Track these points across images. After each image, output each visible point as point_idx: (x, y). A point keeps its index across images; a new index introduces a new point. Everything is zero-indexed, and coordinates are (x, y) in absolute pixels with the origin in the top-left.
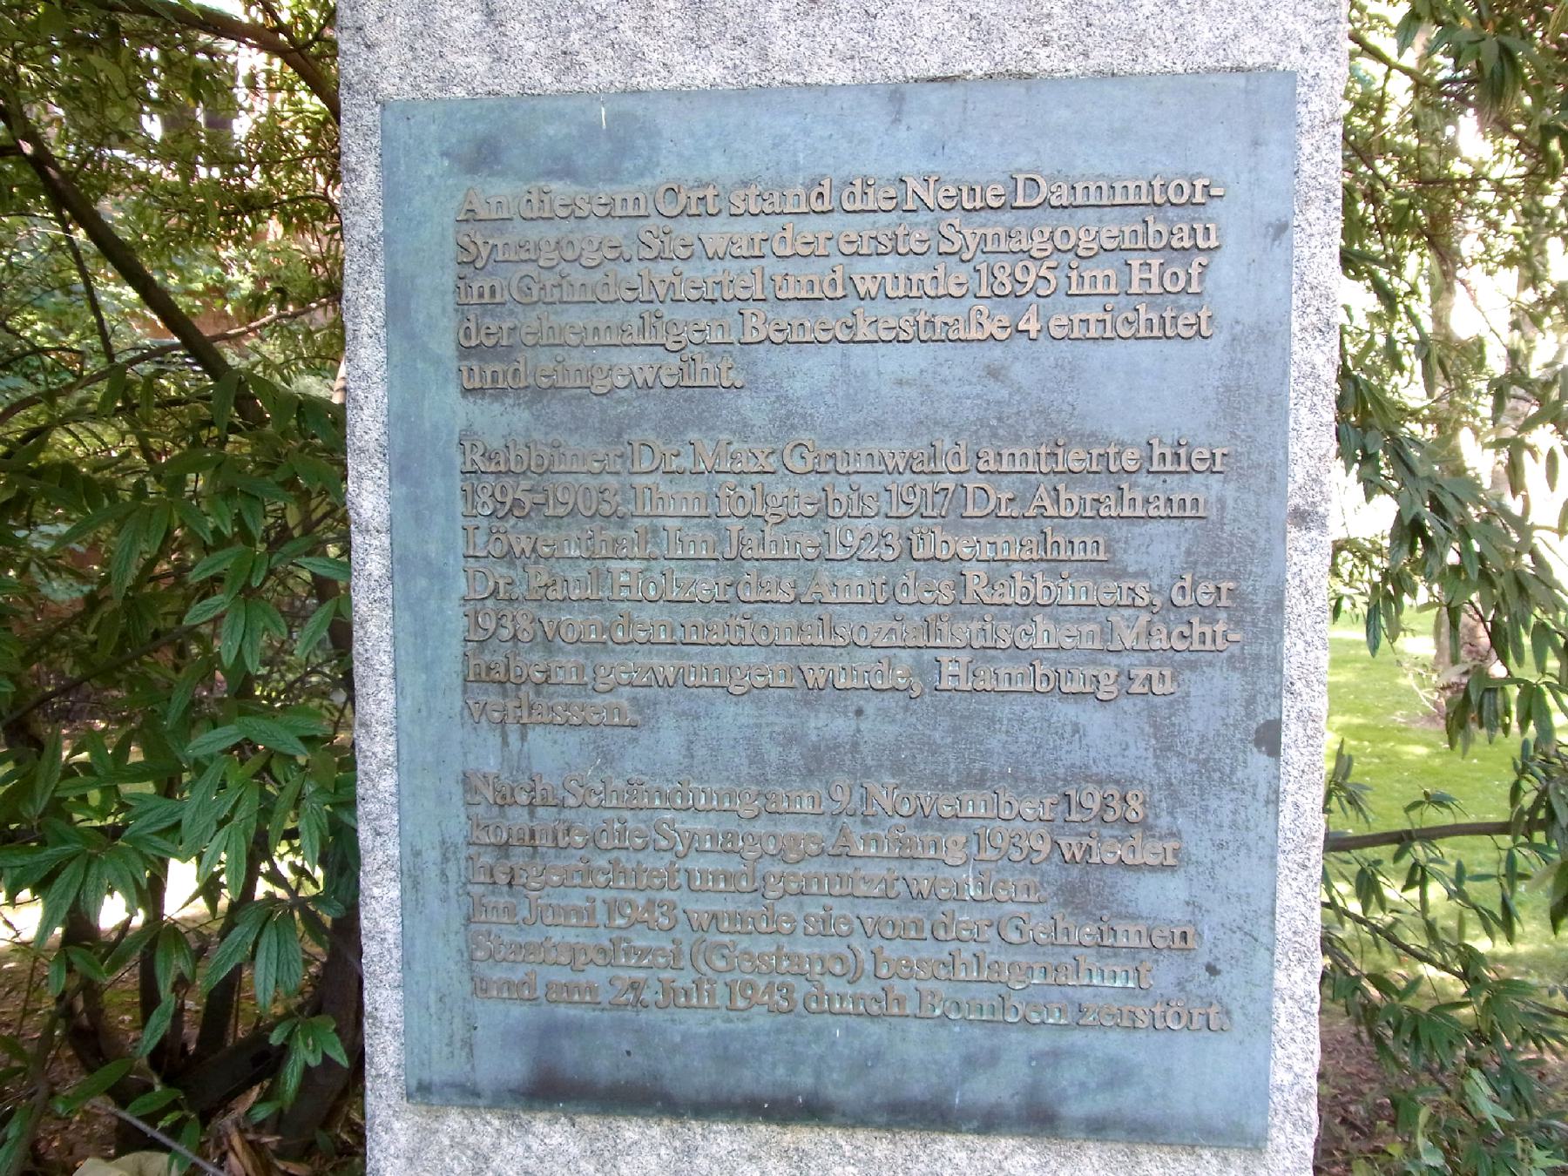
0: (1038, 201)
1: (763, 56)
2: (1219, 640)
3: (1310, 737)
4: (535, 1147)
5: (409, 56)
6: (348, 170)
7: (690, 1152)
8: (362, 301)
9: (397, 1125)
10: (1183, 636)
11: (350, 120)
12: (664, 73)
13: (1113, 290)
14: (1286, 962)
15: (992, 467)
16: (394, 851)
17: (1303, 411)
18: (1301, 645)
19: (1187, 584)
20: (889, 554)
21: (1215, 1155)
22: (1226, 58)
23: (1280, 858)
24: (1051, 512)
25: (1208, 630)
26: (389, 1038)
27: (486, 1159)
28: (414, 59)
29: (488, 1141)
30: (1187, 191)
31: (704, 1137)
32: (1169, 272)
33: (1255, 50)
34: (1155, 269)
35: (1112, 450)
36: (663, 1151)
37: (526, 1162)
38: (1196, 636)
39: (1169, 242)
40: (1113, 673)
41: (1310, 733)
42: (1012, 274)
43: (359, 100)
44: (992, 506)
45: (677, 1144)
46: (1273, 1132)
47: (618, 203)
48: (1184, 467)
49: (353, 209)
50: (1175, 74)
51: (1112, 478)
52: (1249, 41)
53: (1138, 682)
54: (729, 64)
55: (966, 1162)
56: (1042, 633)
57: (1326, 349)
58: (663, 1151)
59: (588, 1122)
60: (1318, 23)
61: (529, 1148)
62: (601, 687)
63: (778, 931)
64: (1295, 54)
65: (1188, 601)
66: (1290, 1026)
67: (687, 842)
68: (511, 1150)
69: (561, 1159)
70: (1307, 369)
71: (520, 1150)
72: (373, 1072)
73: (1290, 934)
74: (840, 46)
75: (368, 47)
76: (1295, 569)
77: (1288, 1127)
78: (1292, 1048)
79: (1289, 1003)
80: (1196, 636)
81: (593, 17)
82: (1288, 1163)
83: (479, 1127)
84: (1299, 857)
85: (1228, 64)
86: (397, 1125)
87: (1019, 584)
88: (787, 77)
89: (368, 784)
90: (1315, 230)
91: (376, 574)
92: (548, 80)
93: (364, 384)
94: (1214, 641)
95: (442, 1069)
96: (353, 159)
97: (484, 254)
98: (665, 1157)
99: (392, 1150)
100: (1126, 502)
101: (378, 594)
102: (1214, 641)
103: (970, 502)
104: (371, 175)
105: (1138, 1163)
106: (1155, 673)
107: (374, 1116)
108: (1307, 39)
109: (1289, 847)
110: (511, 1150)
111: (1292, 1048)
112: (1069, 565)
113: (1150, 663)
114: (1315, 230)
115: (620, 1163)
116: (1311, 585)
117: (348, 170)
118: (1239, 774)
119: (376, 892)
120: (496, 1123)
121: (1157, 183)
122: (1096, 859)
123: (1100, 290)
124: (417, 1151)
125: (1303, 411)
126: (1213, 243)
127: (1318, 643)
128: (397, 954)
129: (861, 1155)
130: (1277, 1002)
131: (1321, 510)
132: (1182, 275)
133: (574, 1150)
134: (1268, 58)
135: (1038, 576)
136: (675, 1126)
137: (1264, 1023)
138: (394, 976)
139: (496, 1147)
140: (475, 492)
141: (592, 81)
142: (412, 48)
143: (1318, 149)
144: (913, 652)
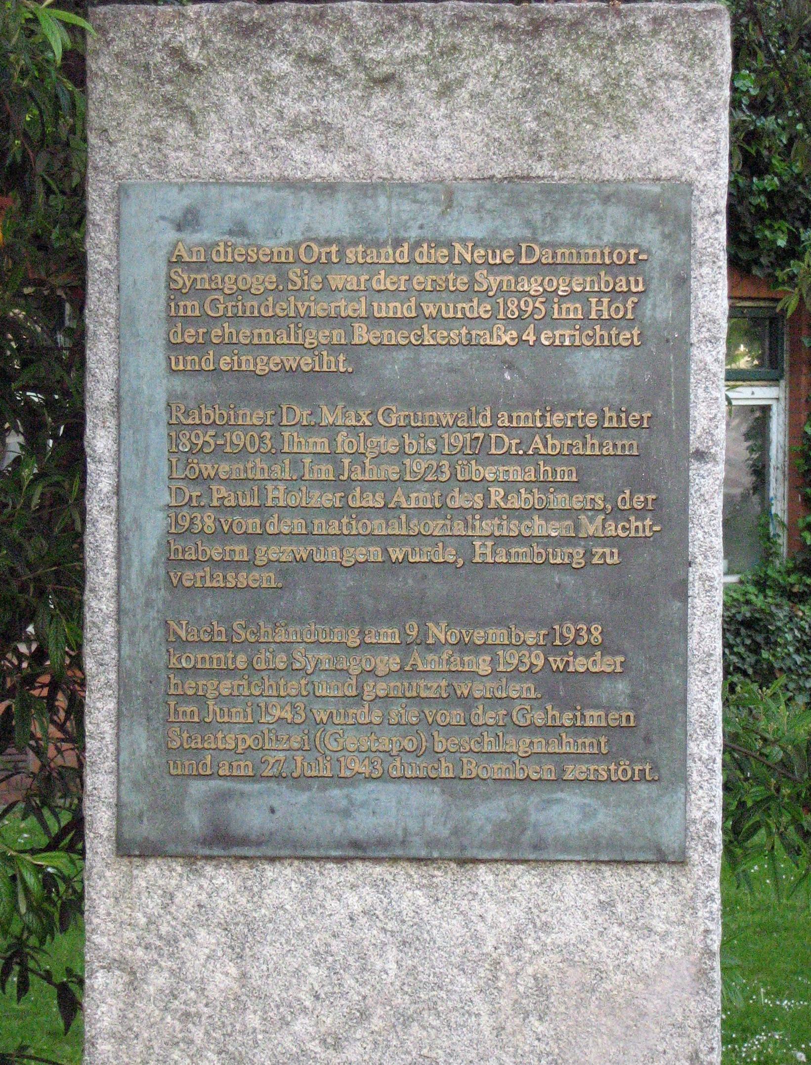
0: (534, 260)
1: (368, 158)
2: (647, 530)
3: (707, 591)
4: (205, 886)
5: (137, 150)
6: (94, 224)
7: (311, 885)
8: (101, 312)
9: (108, 874)
10: (624, 528)
11: (95, 191)
12: (305, 169)
13: (580, 316)
14: (695, 736)
15: (507, 424)
16: (113, 676)
17: (700, 391)
18: (700, 535)
19: (627, 496)
20: (444, 478)
21: (653, 870)
22: (650, 172)
23: (690, 668)
24: (542, 451)
25: (639, 524)
26: (104, 809)
27: (172, 896)
28: (141, 152)
29: (174, 882)
30: (625, 256)
31: (321, 873)
32: (614, 306)
33: (667, 166)
34: (605, 304)
35: (580, 414)
36: (293, 885)
37: (199, 897)
38: (633, 528)
39: (614, 288)
40: (582, 552)
41: (707, 588)
42: (518, 306)
43: (101, 177)
44: (186, 500)
45: (302, 879)
46: (691, 853)
47: (275, 254)
48: (624, 425)
49: (97, 250)
50: (619, 181)
51: (580, 432)
52: (664, 162)
53: (597, 557)
54: (346, 163)
55: (493, 883)
56: (538, 526)
57: (714, 353)
58: (293, 885)
59: (244, 869)
60: (706, 152)
61: (201, 887)
62: (258, 563)
63: (371, 723)
64: (692, 171)
65: (627, 507)
66: (699, 779)
67: (313, 665)
68: (189, 889)
69: (223, 895)
70: (701, 365)
71: (195, 889)
72: (92, 835)
73: (697, 717)
74: (415, 155)
75: (110, 142)
76: (696, 487)
77: (700, 848)
78: (700, 793)
79: (699, 763)
80: (633, 528)
81: (260, 130)
82: (700, 873)
83: (167, 873)
84: (702, 667)
85: (651, 176)
86: (108, 874)
87: (523, 496)
88: (382, 174)
89: (95, 631)
90: (705, 280)
91: (105, 490)
92: (230, 169)
93: (100, 366)
94: (644, 531)
95: (146, 830)
96: (98, 217)
97: (188, 284)
98: (294, 890)
99: (105, 892)
100: (589, 446)
101: (106, 503)
102: (644, 531)
103: (493, 445)
104: (110, 229)
105: (604, 878)
106: (607, 550)
107: (92, 867)
108: (699, 162)
109: (696, 660)
110: (189, 889)
111: (700, 793)
112: (290, 456)
113: (604, 546)
114: (705, 280)
115: (264, 895)
116: (707, 497)
117: (94, 224)
118: (661, 614)
119: (99, 705)
120: (179, 869)
121: (606, 251)
122: (571, 669)
123: (572, 316)
124: (123, 892)
125: (700, 391)
126: (641, 288)
127: (713, 533)
128: (112, 748)
129: (425, 881)
130: (690, 763)
131: (713, 451)
132: (622, 308)
133: (232, 888)
134: (676, 172)
135: (535, 490)
136: (302, 866)
137: (682, 777)
138: (110, 764)
139: (179, 887)
140: (178, 437)
141: (257, 172)
142: (140, 145)
143: (707, 231)
144: (458, 539)
